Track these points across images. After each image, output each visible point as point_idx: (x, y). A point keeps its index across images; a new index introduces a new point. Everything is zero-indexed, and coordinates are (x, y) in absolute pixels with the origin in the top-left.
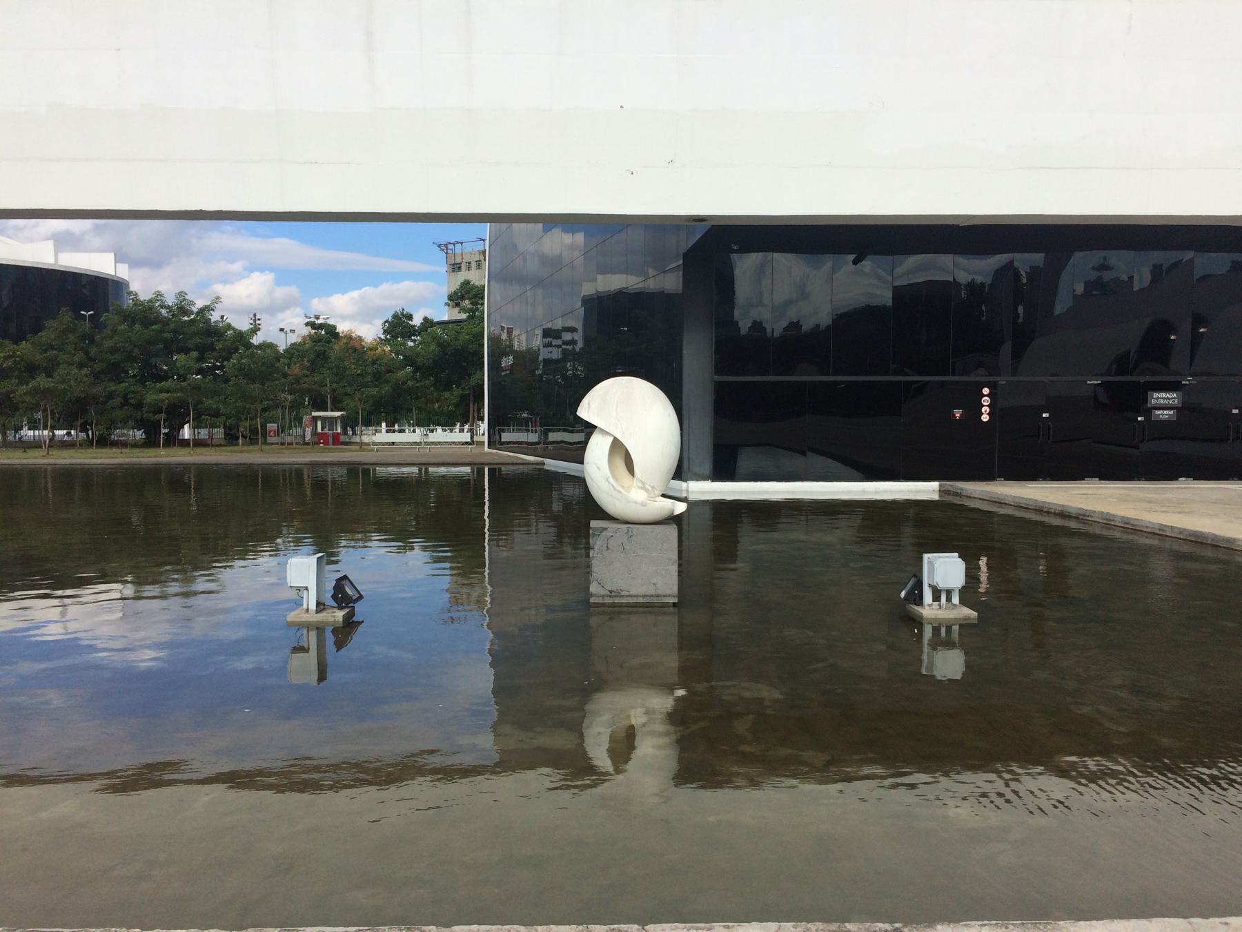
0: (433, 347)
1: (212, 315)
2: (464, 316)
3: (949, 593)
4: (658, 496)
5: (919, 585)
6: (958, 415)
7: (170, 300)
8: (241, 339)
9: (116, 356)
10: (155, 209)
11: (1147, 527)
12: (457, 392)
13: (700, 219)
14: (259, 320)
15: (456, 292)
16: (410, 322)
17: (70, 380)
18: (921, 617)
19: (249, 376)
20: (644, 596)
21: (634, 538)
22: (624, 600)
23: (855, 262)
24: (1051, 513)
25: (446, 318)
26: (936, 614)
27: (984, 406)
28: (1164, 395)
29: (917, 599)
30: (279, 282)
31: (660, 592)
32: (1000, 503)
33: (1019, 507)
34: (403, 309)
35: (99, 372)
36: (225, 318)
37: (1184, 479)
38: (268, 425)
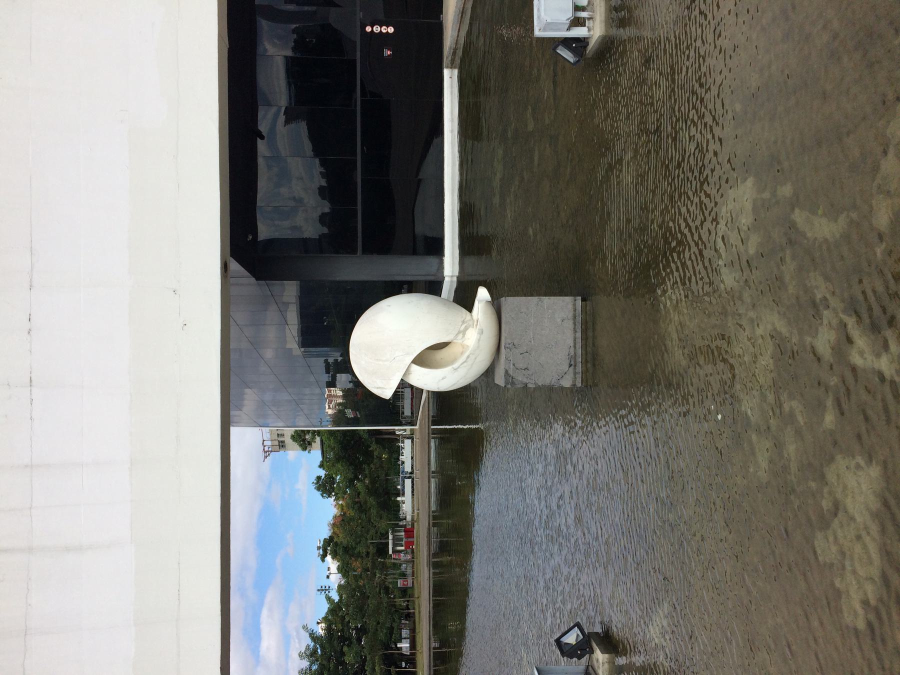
1: (316, 632)
2: (318, 439)
4: (472, 316)
5: (567, 42)
6: (389, 53)
8: (334, 611)
12: (373, 447)
13: (225, 267)
14: (322, 587)
15: (301, 446)
16: (323, 478)
19: (361, 610)
20: (575, 331)
21: (516, 342)
22: (579, 352)
23: (262, 138)
25: (320, 452)
26: (601, 21)
29: (580, 44)
31: (571, 315)
32: (463, 13)
34: (313, 483)
36: (319, 621)
38: (399, 586)
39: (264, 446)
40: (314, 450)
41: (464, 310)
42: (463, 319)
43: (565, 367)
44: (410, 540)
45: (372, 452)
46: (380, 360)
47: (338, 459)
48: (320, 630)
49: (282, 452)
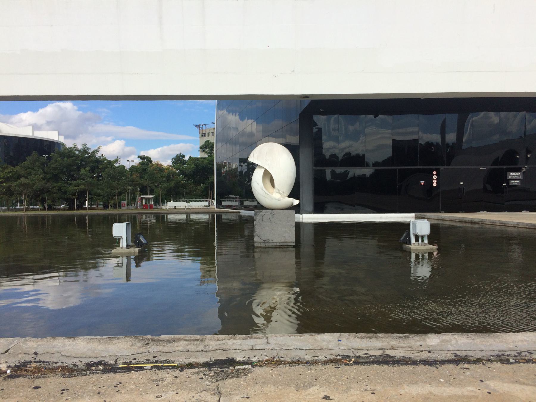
0: (193, 166)
2: (206, 156)
3: (423, 237)
5: (409, 235)
6: (422, 184)
7: (80, 147)
9: (56, 171)
10: (67, 95)
11: (511, 224)
13: (306, 97)
15: (203, 146)
16: (184, 159)
17: (35, 180)
18: (410, 249)
19: (112, 177)
20: (280, 243)
22: (270, 245)
23: (375, 117)
24: (467, 222)
27: (436, 179)
28: (515, 174)
30: (127, 145)
31: (287, 241)
33: (452, 221)
34: (181, 153)
35: (49, 178)
36: (103, 155)
37: (525, 211)
38: (122, 201)
39: (202, 125)
40: (200, 154)
41: (288, 195)
42: (285, 192)
43: (263, 238)
44: (149, 207)
45: (200, 185)
46: (266, 155)
47: (196, 165)
48: (98, 155)
49: (199, 135)
